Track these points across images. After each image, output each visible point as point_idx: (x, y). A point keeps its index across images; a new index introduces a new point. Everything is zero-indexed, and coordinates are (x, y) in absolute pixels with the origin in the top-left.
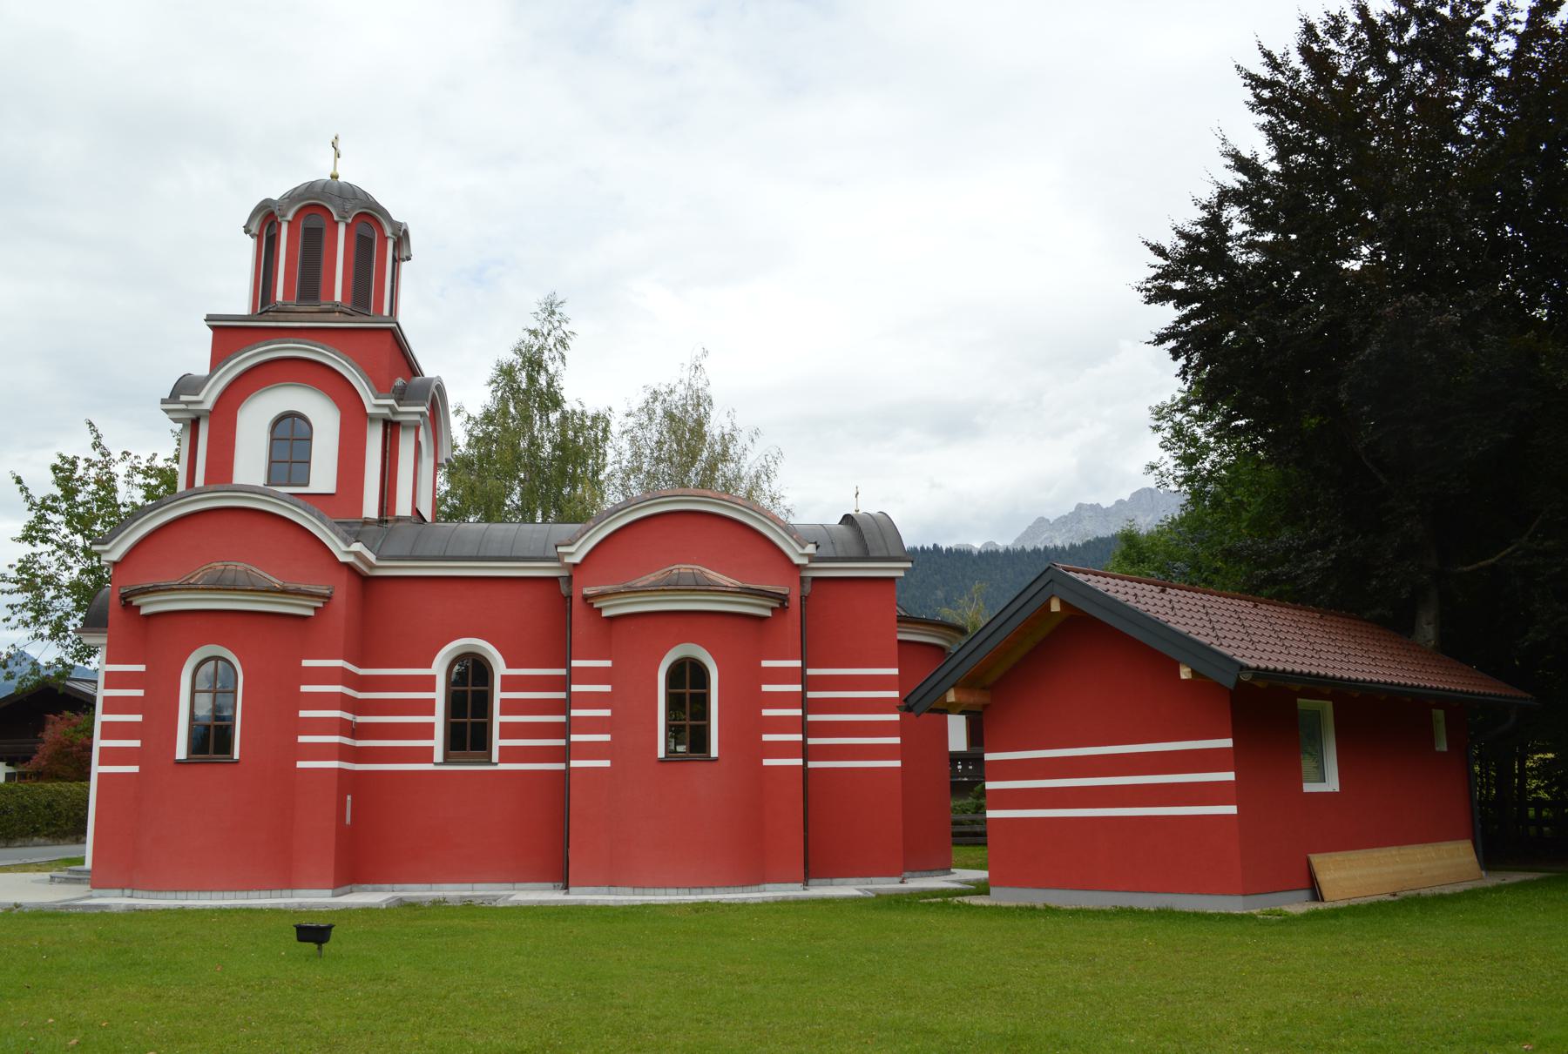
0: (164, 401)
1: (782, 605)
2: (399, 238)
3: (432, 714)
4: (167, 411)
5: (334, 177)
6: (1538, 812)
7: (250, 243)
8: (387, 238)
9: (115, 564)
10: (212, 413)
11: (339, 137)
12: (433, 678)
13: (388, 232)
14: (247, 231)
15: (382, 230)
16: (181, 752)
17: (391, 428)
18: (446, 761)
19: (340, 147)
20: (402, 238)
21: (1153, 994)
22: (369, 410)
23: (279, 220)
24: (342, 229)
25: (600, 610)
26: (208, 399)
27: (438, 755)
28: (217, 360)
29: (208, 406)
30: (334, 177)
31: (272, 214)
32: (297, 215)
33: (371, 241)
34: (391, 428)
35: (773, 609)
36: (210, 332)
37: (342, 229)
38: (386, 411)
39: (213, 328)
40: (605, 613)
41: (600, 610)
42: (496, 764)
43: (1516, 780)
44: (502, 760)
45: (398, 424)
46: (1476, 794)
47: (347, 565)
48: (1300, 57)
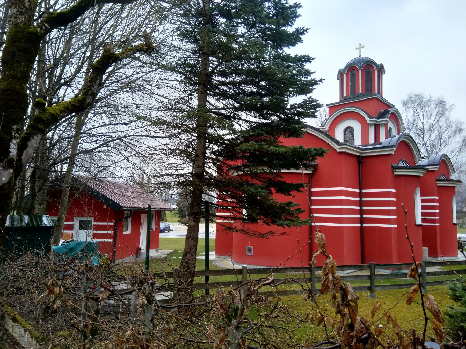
5: (360, 56)
6: (200, 286)
7: (338, 82)
8: (375, 70)
13: (375, 68)
14: (337, 79)
15: (373, 68)
17: (377, 127)
21: (356, 335)
22: (368, 122)
24: (360, 71)
32: (348, 71)
33: (370, 72)
34: (377, 127)
37: (360, 71)
38: (373, 122)
40: (438, 185)
43: (18, 238)
45: (379, 125)
48: (300, 55)
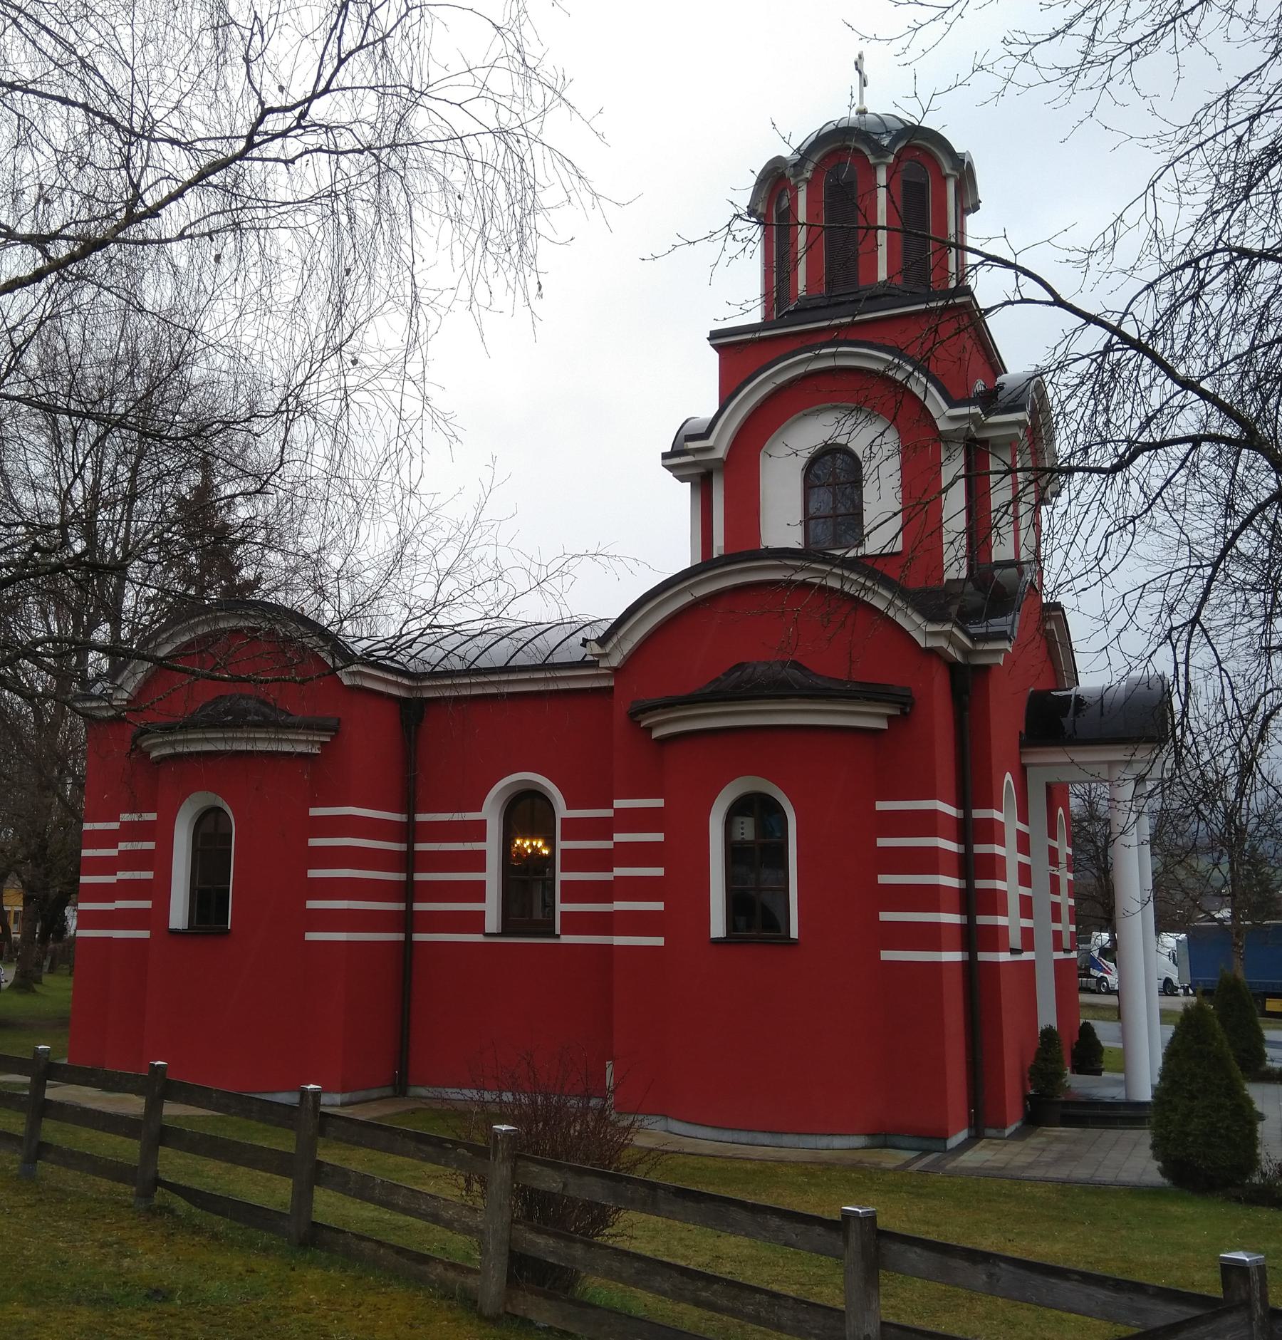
0: (665, 456)
1: (904, 713)
2: (962, 175)
3: (483, 869)
4: (670, 468)
9: (615, 670)
10: (727, 465)
11: (865, 56)
12: (483, 823)
15: (938, 167)
16: (718, 928)
18: (503, 933)
19: (866, 70)
20: (965, 173)
22: (942, 426)
23: (793, 181)
25: (649, 729)
26: (720, 446)
27: (492, 922)
28: (727, 394)
29: (720, 453)
30: (862, 112)
31: (782, 177)
35: (890, 718)
36: (715, 356)
39: (718, 348)
40: (656, 734)
41: (649, 729)
42: (558, 936)
44: (565, 931)
45: (985, 442)
46: (41, 930)
47: (931, 651)
